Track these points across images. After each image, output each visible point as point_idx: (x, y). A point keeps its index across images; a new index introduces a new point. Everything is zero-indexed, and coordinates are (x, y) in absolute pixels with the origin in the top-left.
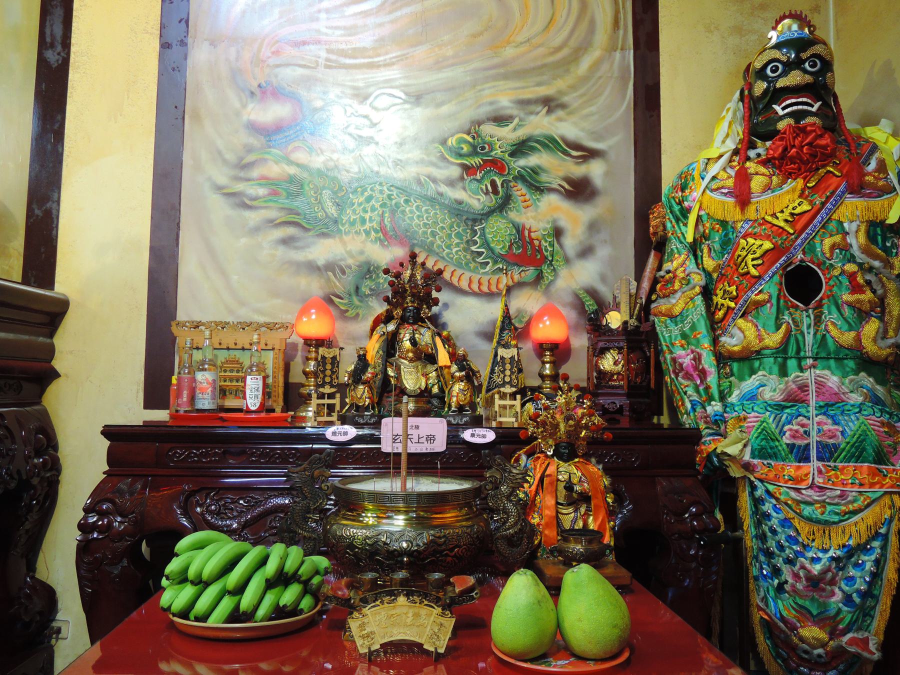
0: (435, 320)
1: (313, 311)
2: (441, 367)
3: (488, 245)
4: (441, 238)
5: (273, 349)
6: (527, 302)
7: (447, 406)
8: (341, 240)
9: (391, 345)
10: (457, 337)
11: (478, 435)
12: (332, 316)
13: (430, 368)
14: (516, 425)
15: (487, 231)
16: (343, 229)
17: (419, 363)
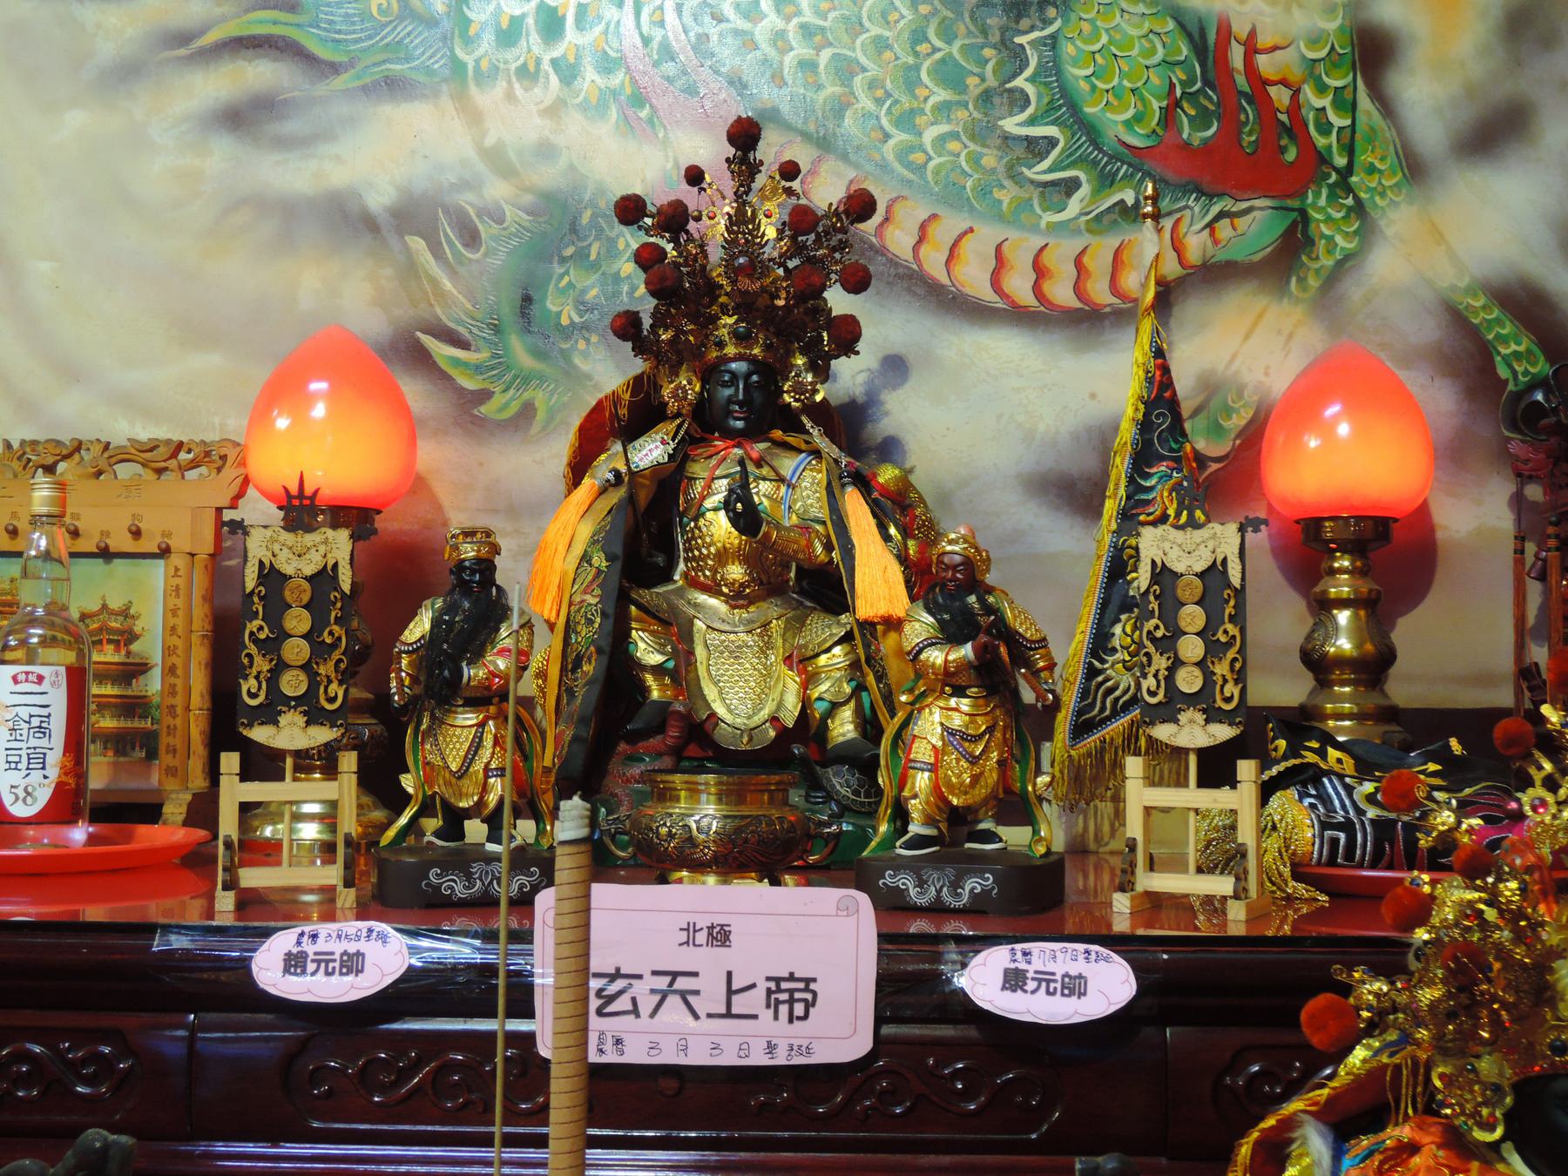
0: (848, 426)
1: (318, 386)
2: (867, 626)
3: (1074, 109)
4: (872, 85)
5: (164, 552)
6: (1243, 349)
7: (885, 810)
8: (461, 97)
9: (646, 538)
10: (945, 498)
11: (1045, 979)
12: (401, 408)
13: (822, 628)
14: (1237, 919)
15: (1068, 49)
16: (469, 60)
17: (771, 610)
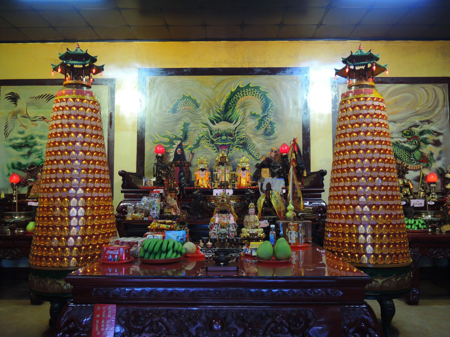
6: (426, 172)
